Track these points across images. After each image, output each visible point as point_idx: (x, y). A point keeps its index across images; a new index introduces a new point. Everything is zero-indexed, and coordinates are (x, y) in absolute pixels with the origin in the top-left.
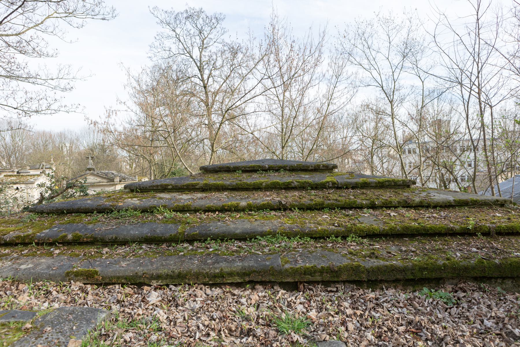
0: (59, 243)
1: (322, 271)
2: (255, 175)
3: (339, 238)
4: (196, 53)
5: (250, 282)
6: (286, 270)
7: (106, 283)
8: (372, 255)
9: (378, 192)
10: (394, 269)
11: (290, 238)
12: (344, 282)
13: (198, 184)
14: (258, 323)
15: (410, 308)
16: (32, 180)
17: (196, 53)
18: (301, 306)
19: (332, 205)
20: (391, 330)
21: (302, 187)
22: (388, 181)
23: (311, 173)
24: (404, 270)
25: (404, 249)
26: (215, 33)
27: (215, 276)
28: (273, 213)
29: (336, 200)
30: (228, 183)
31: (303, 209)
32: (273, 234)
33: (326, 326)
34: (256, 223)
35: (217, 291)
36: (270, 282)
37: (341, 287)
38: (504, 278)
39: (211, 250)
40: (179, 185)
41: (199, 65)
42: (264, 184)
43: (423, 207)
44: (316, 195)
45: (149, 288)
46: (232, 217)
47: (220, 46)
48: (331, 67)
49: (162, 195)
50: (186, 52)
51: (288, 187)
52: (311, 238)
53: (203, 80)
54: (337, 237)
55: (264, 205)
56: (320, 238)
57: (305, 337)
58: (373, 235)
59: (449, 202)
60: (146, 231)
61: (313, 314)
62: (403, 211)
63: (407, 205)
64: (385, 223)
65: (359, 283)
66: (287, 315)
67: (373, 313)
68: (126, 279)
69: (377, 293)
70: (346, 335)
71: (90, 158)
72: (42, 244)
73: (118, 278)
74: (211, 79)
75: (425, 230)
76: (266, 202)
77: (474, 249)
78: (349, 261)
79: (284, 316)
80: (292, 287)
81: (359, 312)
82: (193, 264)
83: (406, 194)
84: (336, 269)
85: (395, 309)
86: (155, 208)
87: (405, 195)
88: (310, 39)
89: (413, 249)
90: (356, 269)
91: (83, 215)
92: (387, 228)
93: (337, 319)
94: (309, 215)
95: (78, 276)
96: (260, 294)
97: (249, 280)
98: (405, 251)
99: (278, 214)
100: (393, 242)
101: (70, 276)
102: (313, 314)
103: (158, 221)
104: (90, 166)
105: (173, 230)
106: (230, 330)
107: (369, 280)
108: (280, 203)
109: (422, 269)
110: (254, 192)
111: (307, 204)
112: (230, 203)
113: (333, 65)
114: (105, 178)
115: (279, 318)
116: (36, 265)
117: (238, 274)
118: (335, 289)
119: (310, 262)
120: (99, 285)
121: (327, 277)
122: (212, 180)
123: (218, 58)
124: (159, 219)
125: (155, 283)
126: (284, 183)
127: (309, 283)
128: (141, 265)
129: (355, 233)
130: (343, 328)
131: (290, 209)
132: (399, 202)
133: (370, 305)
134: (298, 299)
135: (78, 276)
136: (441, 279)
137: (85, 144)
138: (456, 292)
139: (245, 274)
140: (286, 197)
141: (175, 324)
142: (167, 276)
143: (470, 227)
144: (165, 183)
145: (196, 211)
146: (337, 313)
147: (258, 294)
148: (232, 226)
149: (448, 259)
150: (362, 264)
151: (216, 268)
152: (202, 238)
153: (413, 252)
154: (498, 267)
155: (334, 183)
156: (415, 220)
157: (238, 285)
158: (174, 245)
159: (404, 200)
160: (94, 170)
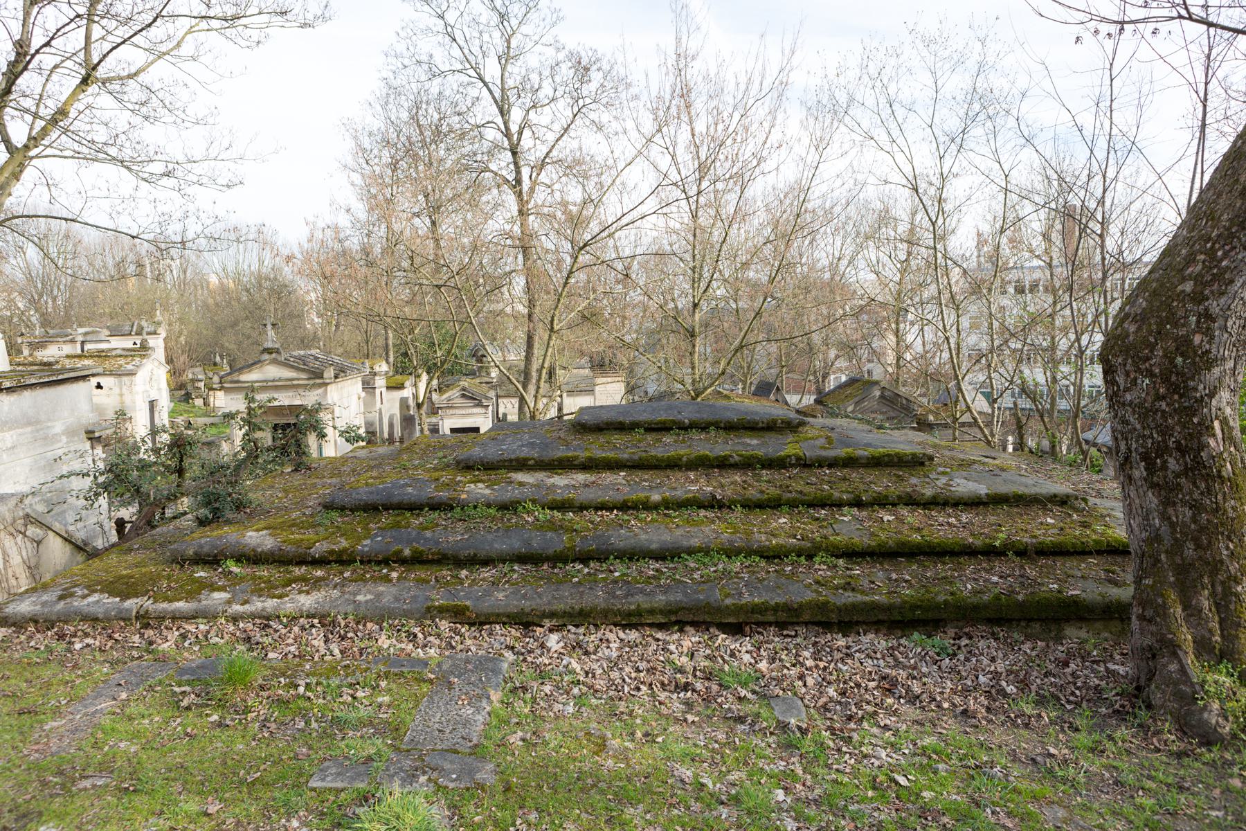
0: (394, 562)
1: (776, 608)
2: (668, 439)
3: (803, 558)
4: (492, 70)
5: (677, 622)
6: (727, 607)
7: (481, 621)
8: (847, 586)
9: (871, 475)
10: (874, 606)
11: (730, 557)
12: (806, 624)
13: (577, 457)
14: (695, 676)
15: (888, 659)
16: (130, 367)
17: (492, 70)
18: (748, 656)
19: (795, 500)
20: (858, 685)
21: (747, 464)
22: (889, 455)
23: (761, 433)
24: (889, 608)
25: (894, 576)
26: (537, 21)
27: (630, 614)
28: (702, 513)
29: (801, 492)
30: (626, 456)
31: (749, 507)
32: (706, 551)
33: (779, 681)
34: (679, 532)
35: (633, 635)
36: (704, 622)
37: (802, 630)
38: (1030, 620)
39: (617, 574)
40: (546, 459)
41: (498, 94)
42: (684, 459)
43: (937, 504)
44: (769, 482)
45: (542, 630)
46: (640, 520)
47: (551, 51)
48: (806, 128)
49: (520, 477)
50: (468, 66)
51: (723, 464)
52: (761, 557)
53: (508, 134)
54: (799, 556)
55: (688, 500)
56: (774, 557)
57: (754, 692)
58: (852, 554)
59: (979, 497)
60: (514, 544)
61: (763, 666)
62: (904, 511)
63: (912, 501)
64: (872, 534)
65: (827, 626)
66: (731, 666)
67: (840, 665)
68: (508, 616)
69: (850, 639)
70: (803, 690)
71: (269, 327)
72: (369, 562)
73: (498, 615)
74: (527, 133)
75: (929, 547)
76: (691, 495)
77: (995, 579)
78: (814, 595)
79: (726, 668)
80: (736, 630)
81: (822, 665)
82: (597, 596)
83: (914, 481)
84: (796, 606)
85: (870, 661)
86: (519, 502)
87: (915, 483)
88: (760, 62)
89: (908, 577)
90: (823, 607)
91: (408, 514)
92: (874, 544)
93: (794, 672)
94: (758, 517)
95: (442, 611)
96: (693, 639)
97: (677, 619)
98: (896, 580)
99: (710, 514)
100: (881, 564)
101: (431, 613)
102: (763, 666)
103: (528, 527)
104: (269, 345)
105: (561, 542)
106: (663, 684)
107: (840, 622)
108: (714, 497)
109: (914, 607)
110: (669, 472)
111: (754, 499)
112: (634, 497)
113: (811, 121)
114: (303, 370)
115: (722, 670)
116: (379, 596)
117: (661, 612)
118: (793, 633)
119: (760, 596)
120: (471, 624)
121: (782, 616)
122: (596, 448)
123: (545, 84)
124: (527, 522)
125: (548, 623)
126: (717, 458)
127: (758, 624)
128: (524, 597)
129: (826, 551)
130: (800, 683)
131: (729, 507)
132: (900, 497)
133: (837, 655)
134: (743, 647)
135: (442, 611)
136: (941, 620)
137: (217, 266)
138: (960, 638)
139: (671, 612)
140: (722, 486)
141: (594, 676)
142: (565, 614)
143: (997, 543)
144: (522, 455)
145: (582, 508)
146: (794, 665)
147: (691, 639)
148: (644, 537)
149: (952, 594)
150: (832, 599)
151: (630, 604)
152: (600, 556)
153: (906, 581)
154: (1021, 605)
155: (798, 458)
156: (919, 530)
157: (661, 627)
158: (561, 565)
159: (908, 493)
160: (278, 352)
